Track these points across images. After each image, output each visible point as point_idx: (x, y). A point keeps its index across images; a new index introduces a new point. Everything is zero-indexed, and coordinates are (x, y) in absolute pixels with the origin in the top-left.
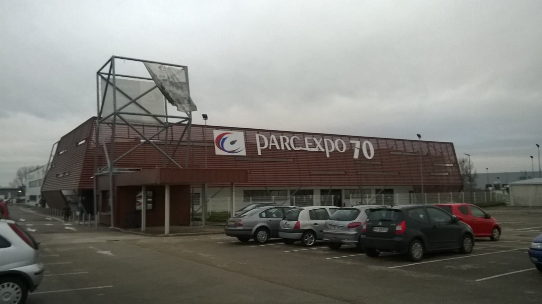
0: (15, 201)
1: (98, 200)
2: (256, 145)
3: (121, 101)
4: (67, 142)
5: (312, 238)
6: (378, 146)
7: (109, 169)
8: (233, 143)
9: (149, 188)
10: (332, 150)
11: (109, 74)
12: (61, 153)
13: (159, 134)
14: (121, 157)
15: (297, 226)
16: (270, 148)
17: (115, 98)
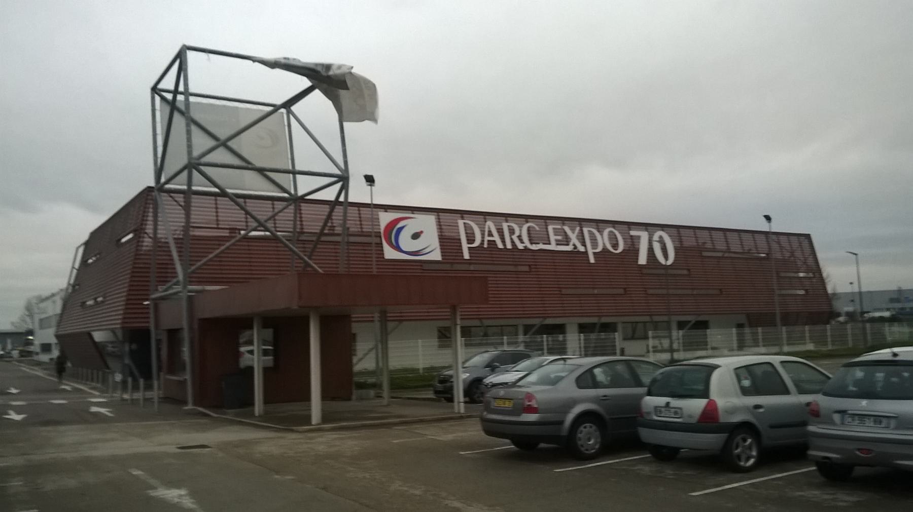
0: (15, 353)
1: (159, 350)
3: (201, 143)
4: (99, 243)
5: (750, 448)
6: (681, 242)
7: (180, 287)
8: (416, 236)
9: (271, 321)
10: (599, 249)
11: (176, 92)
12: (90, 261)
14: (205, 260)
16: (486, 246)
17: (189, 139)
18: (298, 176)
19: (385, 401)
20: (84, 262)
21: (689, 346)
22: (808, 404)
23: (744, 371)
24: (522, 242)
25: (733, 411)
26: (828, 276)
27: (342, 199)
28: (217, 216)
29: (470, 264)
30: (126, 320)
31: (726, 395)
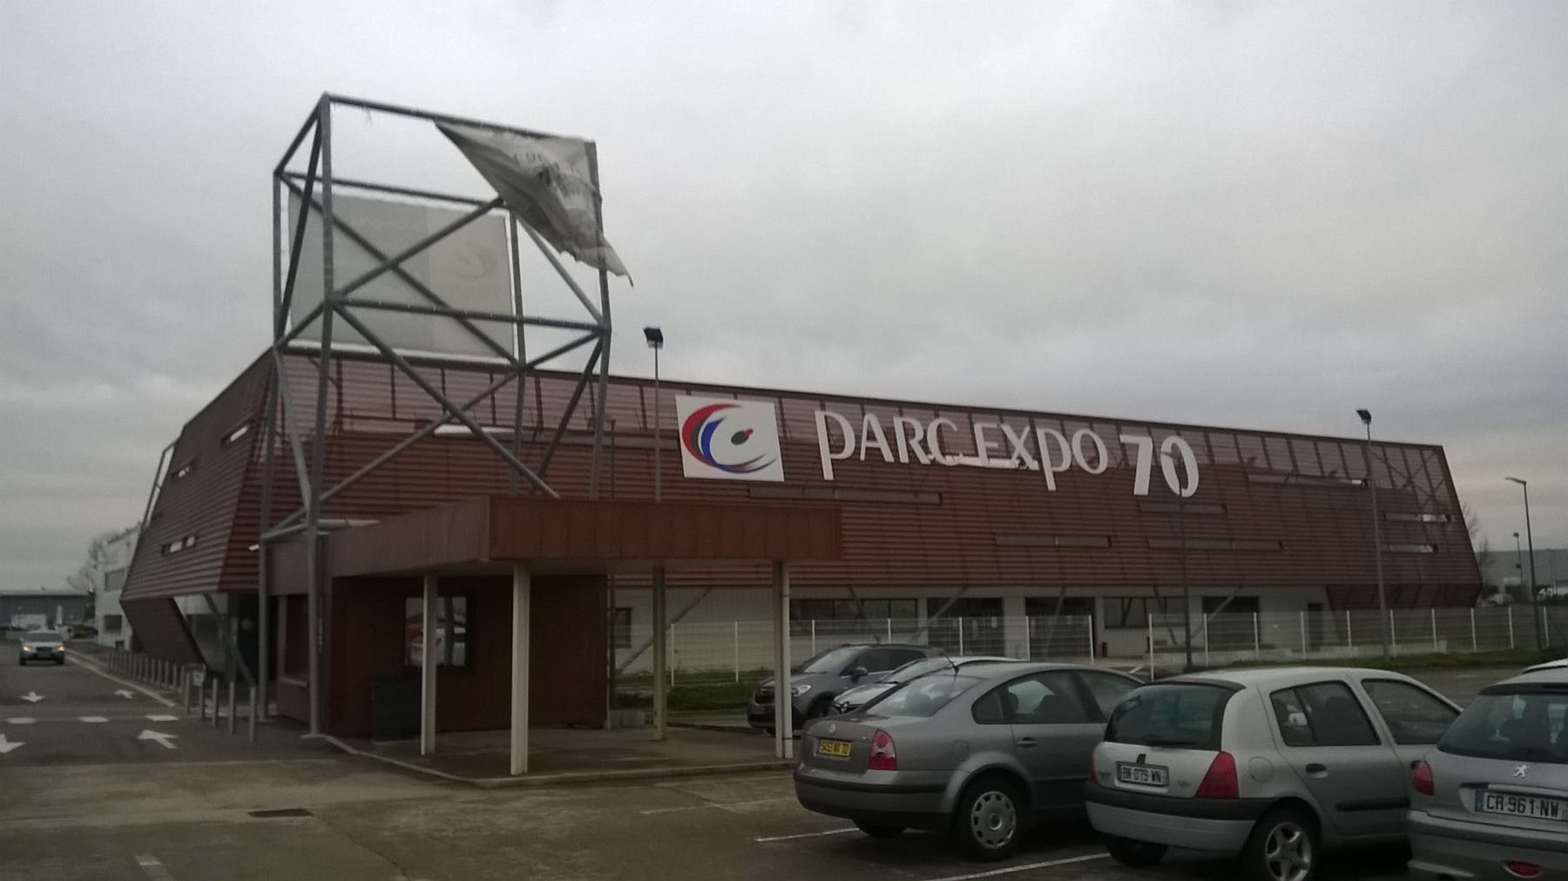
3: (351, 263)
4: (201, 439)
6: (1211, 455)
8: (740, 438)
9: (450, 583)
10: (1065, 466)
11: (311, 177)
12: (182, 473)
13: (492, 392)
15: (1220, 784)
16: (862, 457)
17: (328, 259)
18: (527, 328)
19: (657, 734)
20: (172, 475)
21: (1219, 641)
22: (1414, 765)
23: (1292, 696)
24: (927, 451)
25: (1269, 774)
26: (1474, 521)
27: (597, 370)
28: (393, 399)
29: (835, 488)
30: (227, 578)
31: (1252, 744)
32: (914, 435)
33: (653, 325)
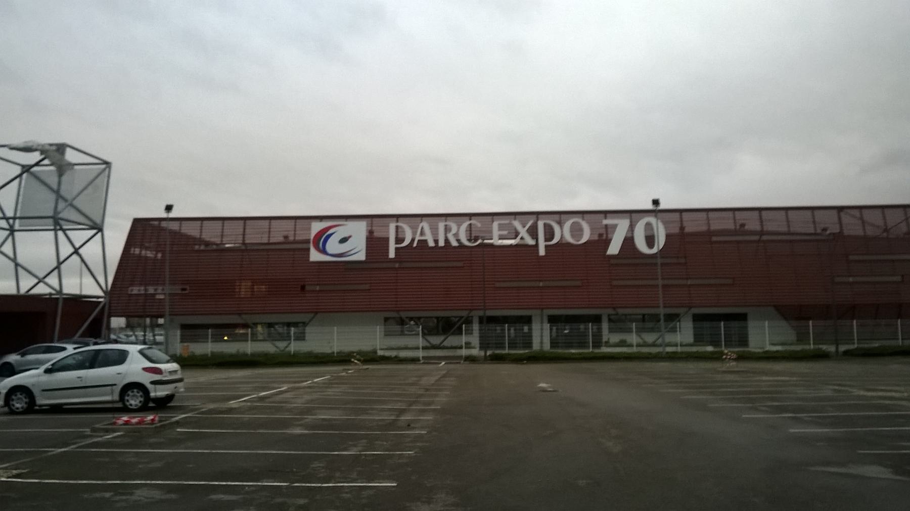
2: (387, 240)
8: (344, 240)
16: (415, 245)
32: (450, 230)
33: (656, 197)
